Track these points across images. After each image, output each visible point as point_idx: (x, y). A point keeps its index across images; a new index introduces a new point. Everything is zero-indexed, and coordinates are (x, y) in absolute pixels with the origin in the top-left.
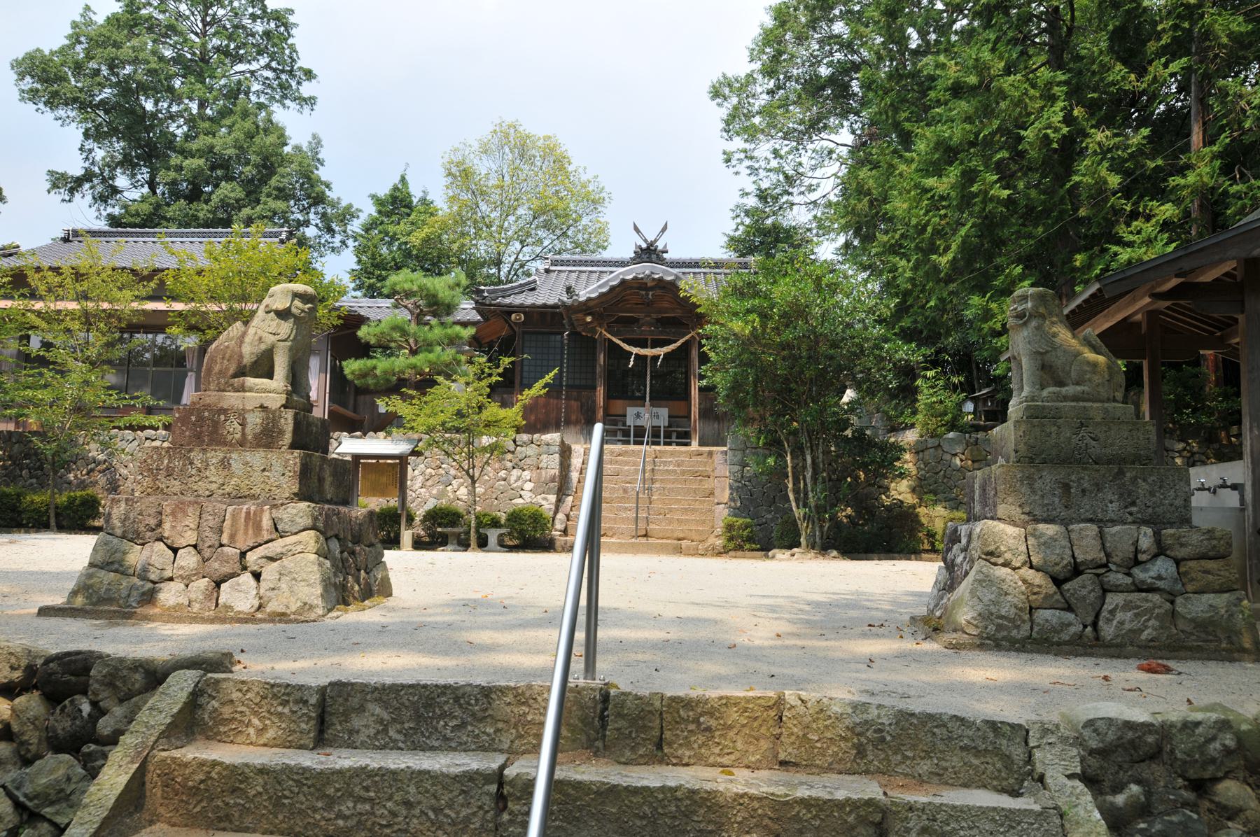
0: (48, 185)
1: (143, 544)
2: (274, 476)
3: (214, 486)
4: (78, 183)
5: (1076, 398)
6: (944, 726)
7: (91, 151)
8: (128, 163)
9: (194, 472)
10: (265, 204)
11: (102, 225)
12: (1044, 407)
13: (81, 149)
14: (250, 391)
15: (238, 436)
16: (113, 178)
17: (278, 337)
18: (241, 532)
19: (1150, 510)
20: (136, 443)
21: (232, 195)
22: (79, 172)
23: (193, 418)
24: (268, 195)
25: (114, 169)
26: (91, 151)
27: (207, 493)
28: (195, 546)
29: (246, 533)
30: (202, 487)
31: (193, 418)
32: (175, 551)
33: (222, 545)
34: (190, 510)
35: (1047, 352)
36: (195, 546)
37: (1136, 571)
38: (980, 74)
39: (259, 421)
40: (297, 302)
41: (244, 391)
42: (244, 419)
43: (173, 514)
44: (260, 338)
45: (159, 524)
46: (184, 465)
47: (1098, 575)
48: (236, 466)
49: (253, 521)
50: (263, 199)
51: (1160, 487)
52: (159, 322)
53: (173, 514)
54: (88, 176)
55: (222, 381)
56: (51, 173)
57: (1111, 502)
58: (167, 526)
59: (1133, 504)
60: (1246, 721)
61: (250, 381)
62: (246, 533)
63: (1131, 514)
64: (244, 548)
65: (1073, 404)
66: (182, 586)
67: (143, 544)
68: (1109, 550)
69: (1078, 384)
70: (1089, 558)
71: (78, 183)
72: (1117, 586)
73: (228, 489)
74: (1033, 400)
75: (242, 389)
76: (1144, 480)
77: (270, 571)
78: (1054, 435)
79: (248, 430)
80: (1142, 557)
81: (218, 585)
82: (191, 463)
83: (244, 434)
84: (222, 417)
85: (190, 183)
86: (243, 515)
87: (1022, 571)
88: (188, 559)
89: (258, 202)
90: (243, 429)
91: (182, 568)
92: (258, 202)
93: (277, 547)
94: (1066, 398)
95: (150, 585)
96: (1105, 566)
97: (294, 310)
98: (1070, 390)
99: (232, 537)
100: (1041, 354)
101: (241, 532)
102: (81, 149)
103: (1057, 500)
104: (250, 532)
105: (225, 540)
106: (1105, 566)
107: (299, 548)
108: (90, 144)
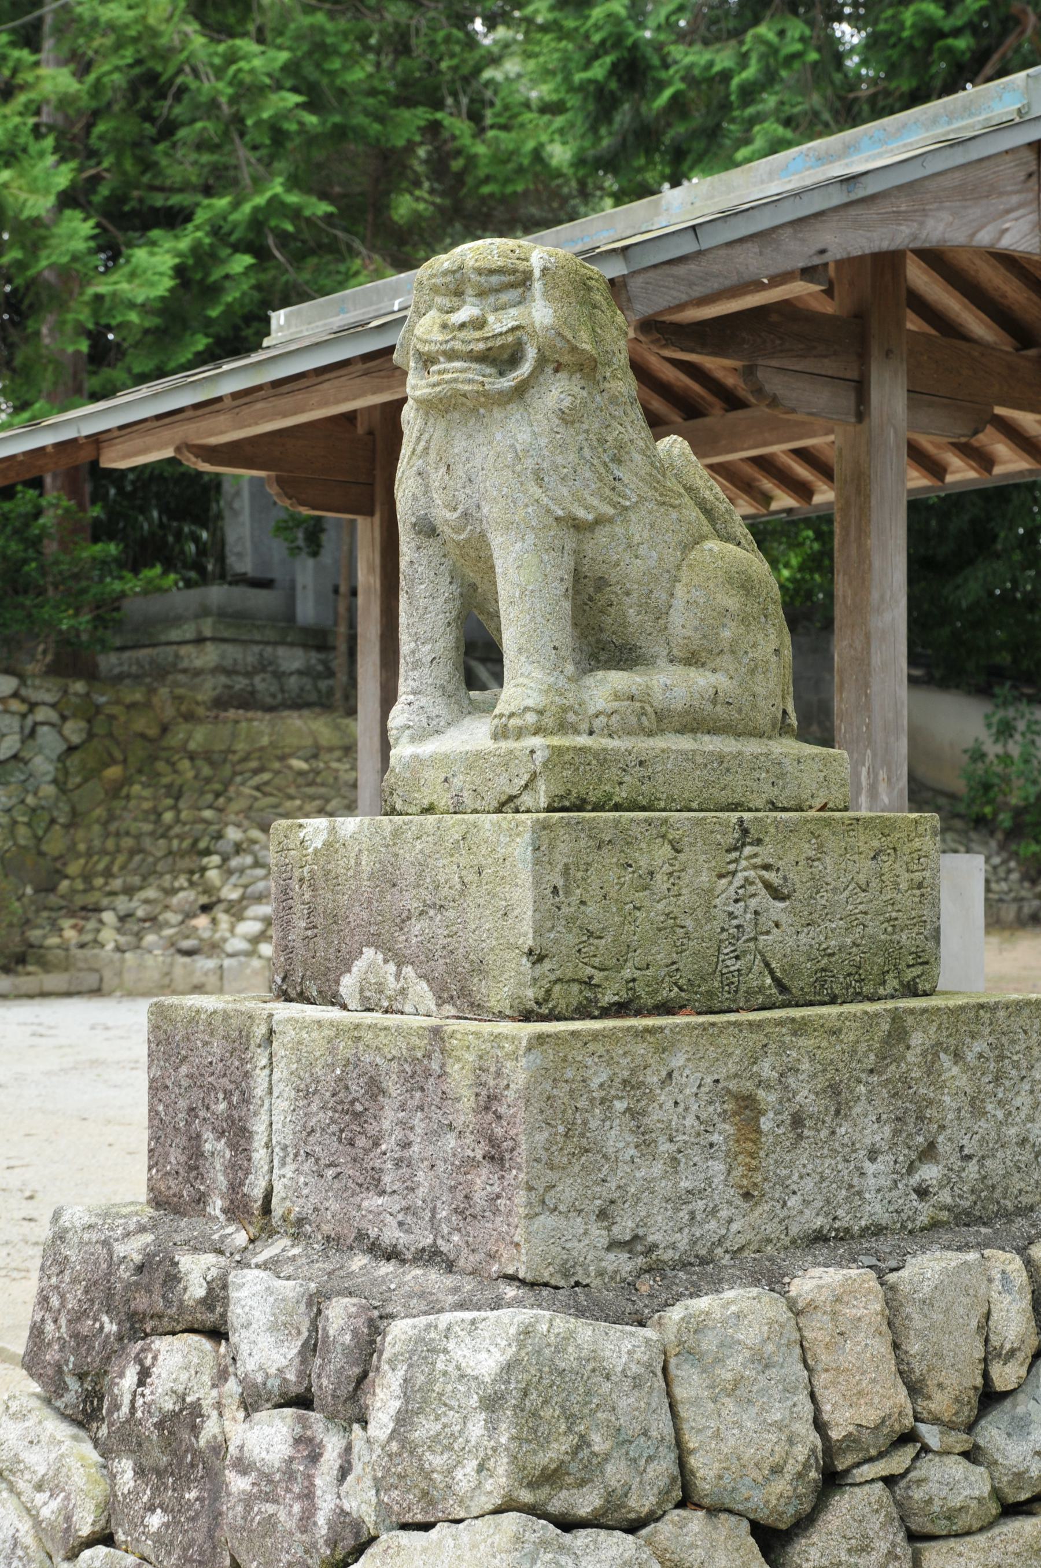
5: (693, 723)
6: (67, 950)
12: (603, 758)
19: (973, 1167)
35: (599, 521)
37: (992, 1434)
38: (182, 41)
47: (890, 1481)
51: (997, 1080)
57: (873, 1155)
59: (929, 1152)
63: (922, 1193)
65: (685, 743)
68: (918, 1369)
69: (692, 659)
70: (870, 1416)
72: (950, 1516)
74: (563, 727)
76: (957, 1056)
78: (661, 883)
80: (1005, 1375)
87: (664, 1530)
94: (663, 721)
96: (908, 1437)
98: (670, 683)
100: (577, 526)
103: (718, 1167)
106: (908, 1437)
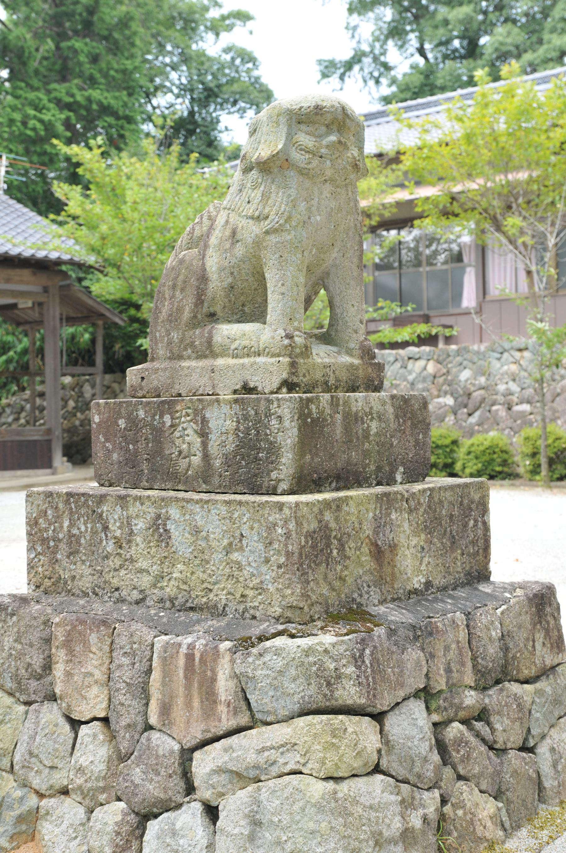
0: (319, 76)
1: (28, 703)
2: (250, 555)
3: (145, 581)
4: (349, 66)
7: (355, 28)
8: (396, 32)
9: (110, 547)
10: (549, 42)
11: (378, 107)
13: (347, 28)
14: (224, 353)
15: (196, 460)
16: (384, 53)
17: (266, 225)
18: (180, 701)
20: (398, 365)
21: (509, 40)
22: (347, 55)
23: (122, 423)
24: (553, 30)
25: (385, 42)
26: (355, 28)
27: (136, 595)
28: (105, 720)
29: (188, 704)
30: (123, 579)
31: (122, 423)
32: (75, 724)
33: (149, 727)
34: (93, 638)
36: (105, 720)
39: (230, 425)
40: (304, 139)
41: (214, 355)
42: (204, 421)
43: (68, 644)
44: (234, 233)
45: (48, 667)
46: (94, 532)
48: (179, 536)
49: (199, 672)
50: (546, 36)
52: (405, 215)
53: (68, 644)
54: (357, 58)
55: (175, 336)
56: (320, 62)
58: (59, 670)
60: (492, 54)
61: (227, 331)
62: (188, 704)
64: (189, 743)
66: (81, 811)
67: (28, 703)
71: (349, 66)
73: (170, 590)
75: (209, 350)
77: (234, 806)
79: (214, 448)
81: (145, 817)
82: (106, 528)
83: (206, 456)
84: (167, 419)
85: (461, 38)
86: (181, 661)
88: (93, 750)
89: (540, 42)
90: (205, 445)
91: (80, 770)
92: (540, 42)
93: (246, 747)
95: (33, 801)
97: (297, 156)
99: (166, 710)
101: (180, 701)
102: (347, 28)
104: (196, 703)
105: (153, 720)
107: (292, 761)
108: (355, 19)
